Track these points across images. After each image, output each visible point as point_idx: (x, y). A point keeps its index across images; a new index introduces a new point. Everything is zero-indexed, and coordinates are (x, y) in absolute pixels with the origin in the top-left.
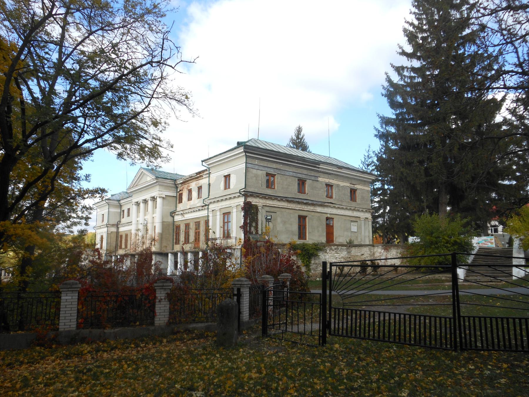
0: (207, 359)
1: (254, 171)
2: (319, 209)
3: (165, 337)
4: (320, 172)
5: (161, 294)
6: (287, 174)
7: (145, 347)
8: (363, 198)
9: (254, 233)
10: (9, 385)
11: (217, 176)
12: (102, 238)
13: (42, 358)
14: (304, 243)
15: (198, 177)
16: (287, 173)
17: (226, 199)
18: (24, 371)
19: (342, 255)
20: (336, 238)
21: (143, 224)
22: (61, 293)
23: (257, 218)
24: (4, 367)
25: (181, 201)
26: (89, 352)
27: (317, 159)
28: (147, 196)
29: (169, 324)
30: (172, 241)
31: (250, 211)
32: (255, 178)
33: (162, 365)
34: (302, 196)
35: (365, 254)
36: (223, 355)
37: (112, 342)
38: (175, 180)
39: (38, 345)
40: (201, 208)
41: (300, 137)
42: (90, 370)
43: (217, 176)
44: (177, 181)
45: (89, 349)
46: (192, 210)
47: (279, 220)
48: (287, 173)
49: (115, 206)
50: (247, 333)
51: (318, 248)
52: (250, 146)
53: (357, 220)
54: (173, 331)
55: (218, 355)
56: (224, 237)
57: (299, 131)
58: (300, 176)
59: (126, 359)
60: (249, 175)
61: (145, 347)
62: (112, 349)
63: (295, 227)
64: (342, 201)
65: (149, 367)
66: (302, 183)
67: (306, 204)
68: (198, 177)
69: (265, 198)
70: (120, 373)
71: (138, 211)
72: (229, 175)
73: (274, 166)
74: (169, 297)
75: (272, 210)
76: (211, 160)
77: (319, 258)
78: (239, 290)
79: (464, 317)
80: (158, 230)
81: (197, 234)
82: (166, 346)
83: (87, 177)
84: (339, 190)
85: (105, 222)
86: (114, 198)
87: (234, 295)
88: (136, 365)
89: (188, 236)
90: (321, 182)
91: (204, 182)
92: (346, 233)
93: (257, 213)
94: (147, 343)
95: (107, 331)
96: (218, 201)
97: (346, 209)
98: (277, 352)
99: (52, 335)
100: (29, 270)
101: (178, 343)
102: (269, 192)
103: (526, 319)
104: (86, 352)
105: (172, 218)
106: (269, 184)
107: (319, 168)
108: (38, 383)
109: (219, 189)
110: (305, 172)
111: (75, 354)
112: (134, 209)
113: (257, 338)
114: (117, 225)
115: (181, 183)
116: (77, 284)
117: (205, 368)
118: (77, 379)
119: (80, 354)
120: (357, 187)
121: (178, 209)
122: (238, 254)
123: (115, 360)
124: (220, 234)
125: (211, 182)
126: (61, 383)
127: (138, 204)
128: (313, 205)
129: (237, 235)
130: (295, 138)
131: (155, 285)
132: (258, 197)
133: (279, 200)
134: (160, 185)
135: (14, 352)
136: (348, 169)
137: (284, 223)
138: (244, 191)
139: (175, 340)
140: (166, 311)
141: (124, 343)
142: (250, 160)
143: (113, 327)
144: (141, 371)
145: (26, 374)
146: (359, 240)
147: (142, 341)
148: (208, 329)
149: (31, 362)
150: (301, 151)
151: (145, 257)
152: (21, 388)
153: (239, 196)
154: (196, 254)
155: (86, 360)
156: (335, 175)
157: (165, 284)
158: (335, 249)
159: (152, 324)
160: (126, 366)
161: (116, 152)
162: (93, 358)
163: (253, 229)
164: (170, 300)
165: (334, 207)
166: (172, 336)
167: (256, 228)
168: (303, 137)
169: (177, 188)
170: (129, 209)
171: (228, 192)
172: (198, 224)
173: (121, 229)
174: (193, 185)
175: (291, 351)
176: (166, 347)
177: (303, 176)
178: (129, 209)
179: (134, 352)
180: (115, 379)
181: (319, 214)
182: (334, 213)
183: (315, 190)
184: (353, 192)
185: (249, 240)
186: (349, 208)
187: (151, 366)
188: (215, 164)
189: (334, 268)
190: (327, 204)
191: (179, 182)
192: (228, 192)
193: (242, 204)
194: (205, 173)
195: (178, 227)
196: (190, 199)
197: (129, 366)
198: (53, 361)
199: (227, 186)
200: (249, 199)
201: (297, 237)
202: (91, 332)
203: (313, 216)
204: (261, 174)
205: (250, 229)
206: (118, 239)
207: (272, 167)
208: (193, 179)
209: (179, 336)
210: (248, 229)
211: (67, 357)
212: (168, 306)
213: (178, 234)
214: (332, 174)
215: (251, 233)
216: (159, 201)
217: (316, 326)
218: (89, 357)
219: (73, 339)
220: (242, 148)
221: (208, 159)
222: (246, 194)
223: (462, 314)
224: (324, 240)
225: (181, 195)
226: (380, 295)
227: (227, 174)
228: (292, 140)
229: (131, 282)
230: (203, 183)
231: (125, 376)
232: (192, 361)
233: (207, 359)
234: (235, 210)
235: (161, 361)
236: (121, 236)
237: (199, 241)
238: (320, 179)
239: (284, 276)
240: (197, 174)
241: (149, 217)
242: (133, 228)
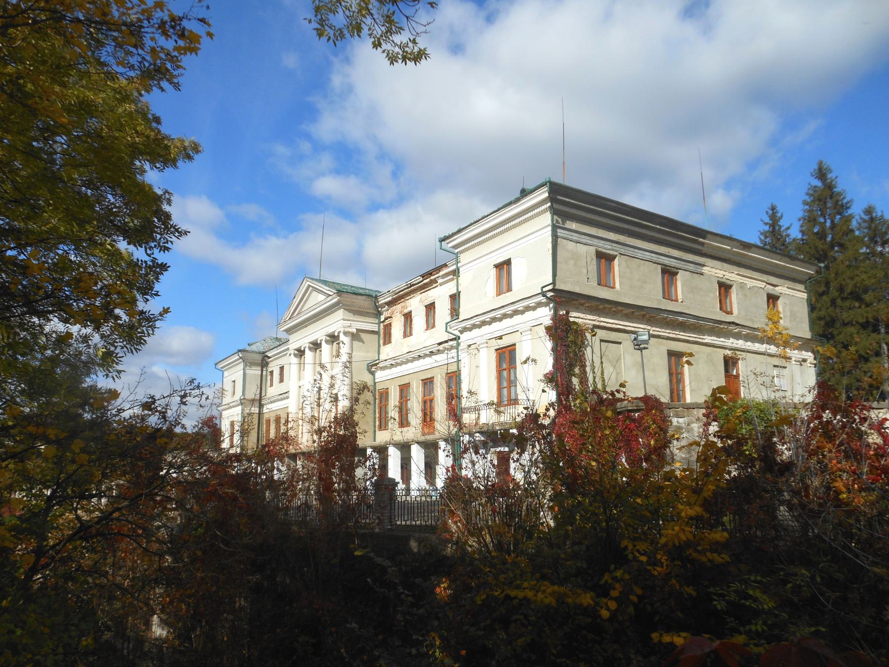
1: (571, 245)
16: (639, 254)
25: (388, 339)
30: (372, 423)
31: (566, 340)
32: (572, 262)
72: (508, 262)
76: (472, 228)
84: (745, 295)
106: (604, 280)
107: (703, 244)
114: (259, 402)
120: (779, 290)
127: (300, 353)
142: (566, 216)
170: (282, 368)
174: (416, 304)
177: (673, 263)
178: (282, 368)
191: (382, 301)
192: (507, 298)
193: (548, 322)
194: (442, 273)
196: (408, 332)
204: (586, 252)
213: (383, 409)
225: (388, 328)
229: (306, 494)
236: (268, 421)
237: (432, 420)
238: (705, 270)
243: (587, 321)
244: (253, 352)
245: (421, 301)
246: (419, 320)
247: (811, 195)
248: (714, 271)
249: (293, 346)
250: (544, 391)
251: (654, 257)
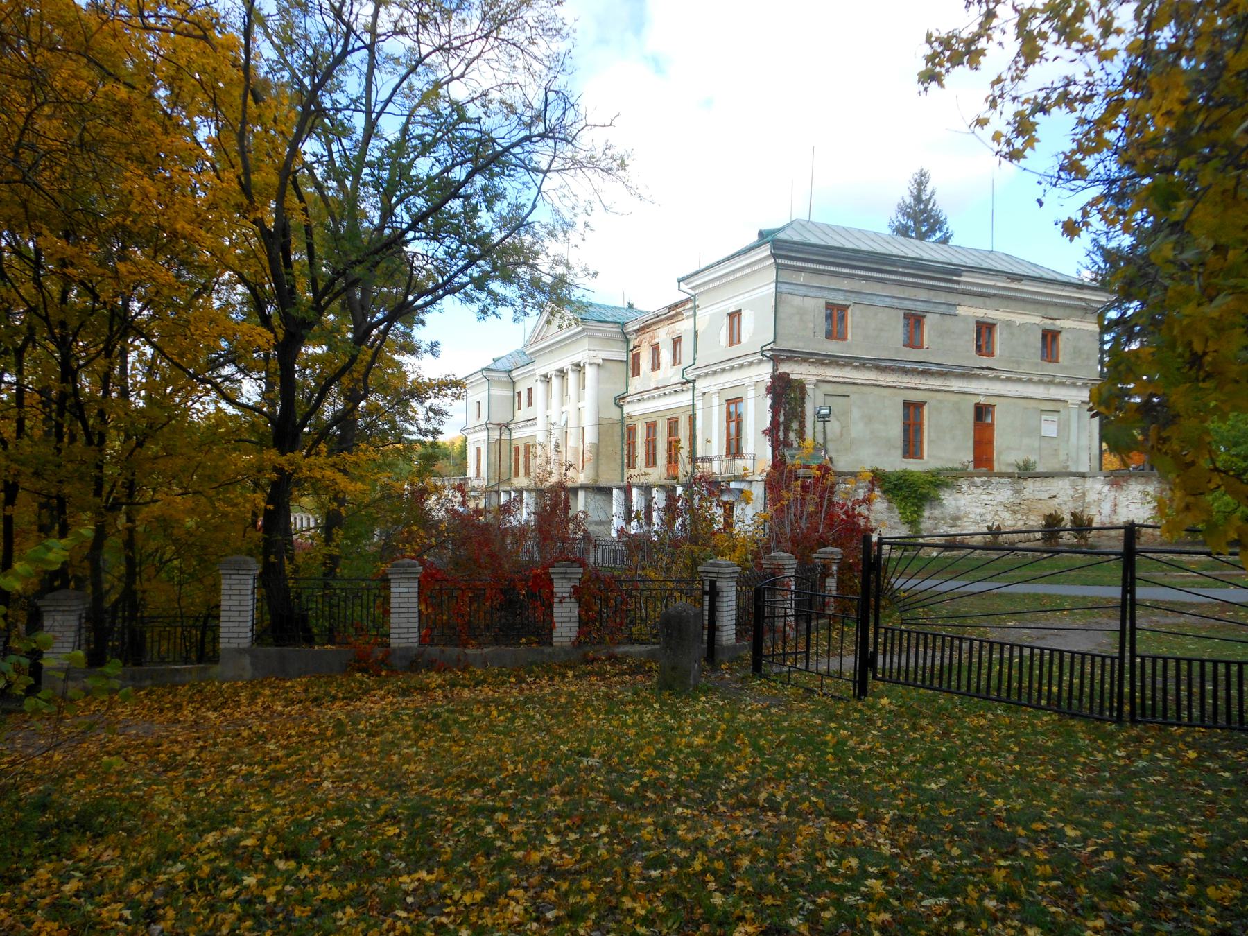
0: (635, 711)
1: (797, 301)
2: (956, 385)
3: (571, 668)
4: (963, 293)
5: (562, 589)
6: (877, 303)
7: (535, 683)
8: (1077, 352)
9: (795, 445)
10: (316, 730)
11: (711, 315)
12: (479, 450)
13: (366, 692)
14: (905, 471)
15: (672, 317)
16: (877, 301)
17: (732, 368)
18: (338, 711)
19: (1000, 498)
20: (1000, 453)
21: (563, 425)
22: (389, 580)
23: (803, 411)
24: (307, 704)
25: (636, 372)
26: (439, 686)
27: (955, 261)
28: (566, 362)
29: (578, 644)
31: (785, 395)
32: (797, 318)
33: (554, 716)
34: (914, 355)
35: (1060, 497)
36: (667, 705)
37: (479, 672)
38: (624, 324)
39: (359, 671)
40: (679, 388)
41: (924, 197)
42: (437, 716)
43: (711, 315)
44: (628, 326)
45: (439, 681)
46: (661, 391)
47: (856, 413)
48: (877, 301)
49: (501, 383)
50: (729, 668)
51: (941, 481)
52: (785, 241)
53: (1059, 406)
54: (587, 655)
55: (656, 706)
56: (728, 453)
57: (921, 181)
58: (910, 305)
59: (497, 702)
60: (785, 311)
61: (535, 683)
62: (478, 684)
63: (896, 430)
64: (1018, 363)
65: (533, 717)
66: (914, 321)
67: (924, 373)
68: (672, 317)
69: (822, 363)
70: (484, 723)
71: (548, 395)
72: (739, 313)
73: (846, 284)
74: (577, 592)
75: (840, 391)
77: (942, 506)
78: (713, 583)
79: (1143, 658)
80: (590, 437)
81: (673, 448)
82: (571, 684)
83: (434, 349)
84: (1012, 334)
85: (484, 419)
86: (499, 365)
87: (705, 593)
88: (513, 712)
89: (654, 448)
90: (966, 317)
91: (683, 327)
92: (1026, 441)
93: (803, 398)
94: (537, 677)
95: (470, 651)
96: (715, 372)
97: (1030, 381)
98: (769, 707)
99: (379, 653)
100: (338, 533)
101: (593, 680)
102: (834, 348)
103: (1241, 665)
104: (434, 685)
105: (619, 410)
107: (958, 282)
108: (358, 731)
109: (716, 346)
110: (923, 295)
111: (416, 689)
112: (539, 390)
113: (743, 680)
115: (636, 331)
116: (414, 566)
117: (624, 724)
118: (416, 728)
119: (424, 690)
121: (632, 390)
122: (758, 491)
123: (479, 702)
125: (700, 328)
126: (392, 732)
127: (546, 379)
128: (941, 374)
129: (758, 453)
130: (909, 200)
131: (551, 570)
132: (805, 360)
133: (856, 367)
134: (590, 337)
135: (322, 680)
136: (1040, 280)
137: (869, 420)
138: (771, 350)
139: (589, 674)
141: (498, 675)
142: (786, 276)
143: (480, 645)
144: (518, 723)
145: (341, 716)
146: (1062, 457)
147: (530, 672)
148: (652, 656)
149: (350, 698)
150: (917, 242)
151: (556, 501)
152: (333, 737)
153: (760, 361)
154: (669, 491)
155: (435, 700)
156: (1002, 297)
157: (569, 570)
158: (984, 483)
159: (551, 644)
160: (495, 713)
161: (475, 307)
162: (445, 697)
163: (792, 436)
164: (579, 601)
165: (997, 378)
166: (583, 667)
167: (801, 435)
168: (933, 194)
169: (628, 341)
170: (530, 390)
171: (737, 350)
172: (673, 424)
173: (517, 434)
174: (663, 335)
175: (796, 705)
176: (570, 686)
177: (919, 307)
178: (530, 390)
179: (515, 692)
180: (475, 733)
181: (956, 398)
182: (995, 392)
183: (947, 339)
184: (1050, 338)
185: (783, 462)
186: (1036, 378)
187: (537, 716)
188: (707, 287)
189: (886, 548)
190: (978, 372)
191: (631, 327)
192: (737, 350)
193: (768, 380)
195: (632, 431)
196: (656, 366)
197: (500, 713)
198: (383, 698)
199: (734, 337)
200: (784, 368)
201: (900, 452)
202: (442, 652)
203: (940, 401)
204: (815, 306)
205: (786, 435)
206: (511, 455)
207: (839, 288)
209: (596, 666)
210: (782, 438)
211: (405, 692)
212: (577, 610)
213: (632, 445)
214: (995, 295)
215: (788, 445)
216: (590, 372)
217: (849, 662)
218: (439, 694)
219: (414, 663)
220: (768, 246)
221: (696, 274)
222: (777, 356)
223: (1140, 649)
224: (968, 456)
225: (636, 357)
226: (1063, 598)
227: (732, 310)
228: (904, 210)
230: (683, 329)
231: (491, 728)
232: (607, 713)
233: (635, 711)
234: (751, 393)
235: (555, 709)
236: (517, 449)
237: (676, 462)
238: (961, 310)
239: (825, 552)
240: (670, 308)
241: (570, 408)
242: (538, 432)
244: (498, 371)
245: (668, 333)
248: (973, 310)
249: (541, 371)
251: (896, 302)
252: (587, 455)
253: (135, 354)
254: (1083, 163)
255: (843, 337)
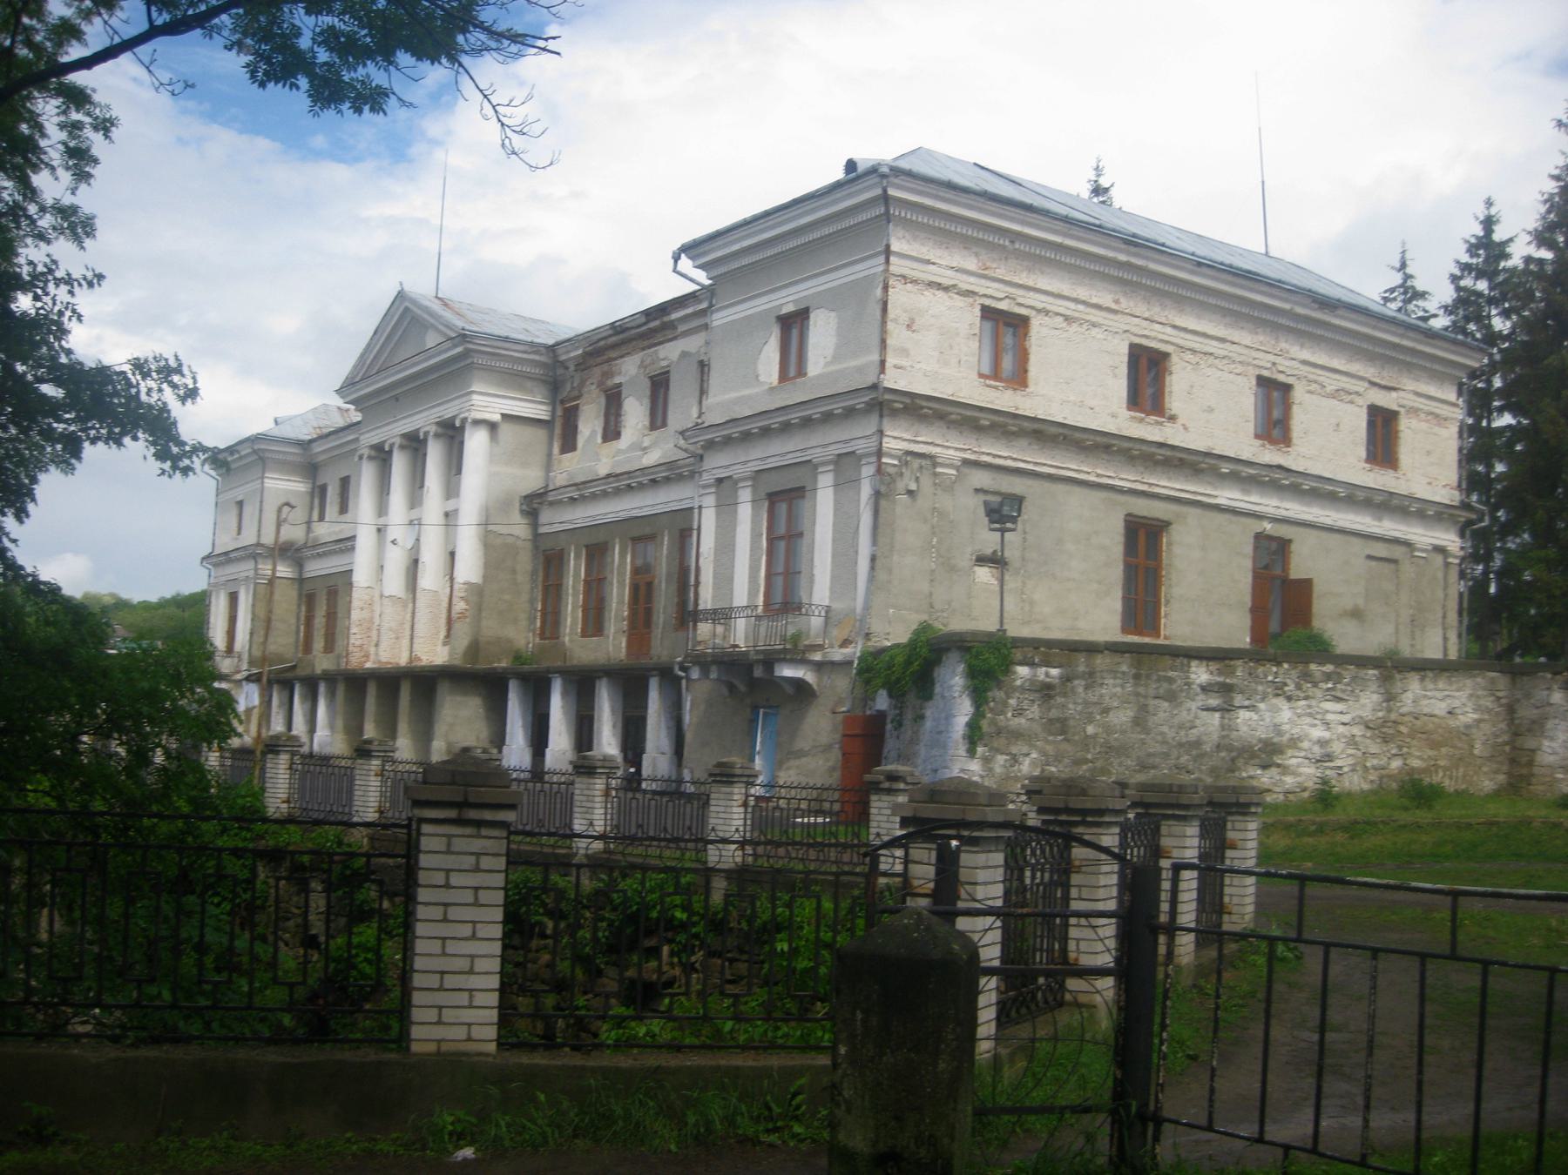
25: (569, 445)
68: (654, 331)
80: (469, 569)
124: (752, 592)
140: (480, 965)
158: (1328, 677)
171: (797, 394)
174: (629, 369)
196: (612, 432)
208: (630, 340)
240: (649, 314)
243: (951, 452)
245: (642, 366)
246: (635, 412)
247: (1557, 178)
250: (1429, 453)
252: (460, 606)
253: (159, 751)
254: (439, 751)
255: (1020, 379)
